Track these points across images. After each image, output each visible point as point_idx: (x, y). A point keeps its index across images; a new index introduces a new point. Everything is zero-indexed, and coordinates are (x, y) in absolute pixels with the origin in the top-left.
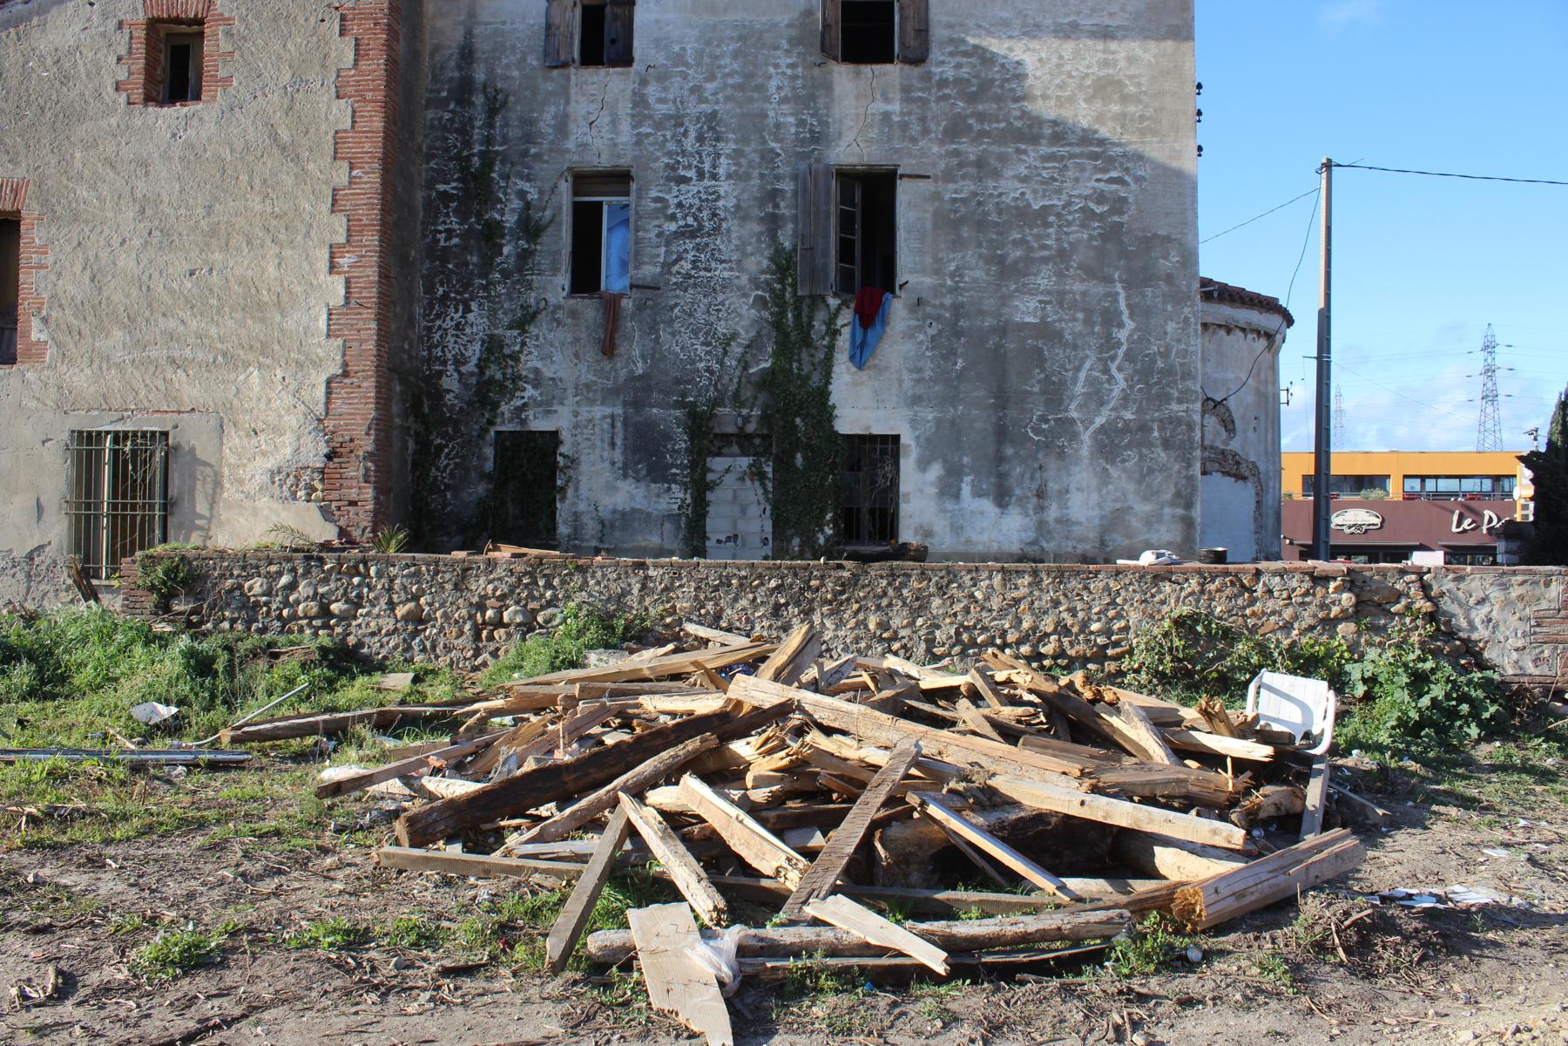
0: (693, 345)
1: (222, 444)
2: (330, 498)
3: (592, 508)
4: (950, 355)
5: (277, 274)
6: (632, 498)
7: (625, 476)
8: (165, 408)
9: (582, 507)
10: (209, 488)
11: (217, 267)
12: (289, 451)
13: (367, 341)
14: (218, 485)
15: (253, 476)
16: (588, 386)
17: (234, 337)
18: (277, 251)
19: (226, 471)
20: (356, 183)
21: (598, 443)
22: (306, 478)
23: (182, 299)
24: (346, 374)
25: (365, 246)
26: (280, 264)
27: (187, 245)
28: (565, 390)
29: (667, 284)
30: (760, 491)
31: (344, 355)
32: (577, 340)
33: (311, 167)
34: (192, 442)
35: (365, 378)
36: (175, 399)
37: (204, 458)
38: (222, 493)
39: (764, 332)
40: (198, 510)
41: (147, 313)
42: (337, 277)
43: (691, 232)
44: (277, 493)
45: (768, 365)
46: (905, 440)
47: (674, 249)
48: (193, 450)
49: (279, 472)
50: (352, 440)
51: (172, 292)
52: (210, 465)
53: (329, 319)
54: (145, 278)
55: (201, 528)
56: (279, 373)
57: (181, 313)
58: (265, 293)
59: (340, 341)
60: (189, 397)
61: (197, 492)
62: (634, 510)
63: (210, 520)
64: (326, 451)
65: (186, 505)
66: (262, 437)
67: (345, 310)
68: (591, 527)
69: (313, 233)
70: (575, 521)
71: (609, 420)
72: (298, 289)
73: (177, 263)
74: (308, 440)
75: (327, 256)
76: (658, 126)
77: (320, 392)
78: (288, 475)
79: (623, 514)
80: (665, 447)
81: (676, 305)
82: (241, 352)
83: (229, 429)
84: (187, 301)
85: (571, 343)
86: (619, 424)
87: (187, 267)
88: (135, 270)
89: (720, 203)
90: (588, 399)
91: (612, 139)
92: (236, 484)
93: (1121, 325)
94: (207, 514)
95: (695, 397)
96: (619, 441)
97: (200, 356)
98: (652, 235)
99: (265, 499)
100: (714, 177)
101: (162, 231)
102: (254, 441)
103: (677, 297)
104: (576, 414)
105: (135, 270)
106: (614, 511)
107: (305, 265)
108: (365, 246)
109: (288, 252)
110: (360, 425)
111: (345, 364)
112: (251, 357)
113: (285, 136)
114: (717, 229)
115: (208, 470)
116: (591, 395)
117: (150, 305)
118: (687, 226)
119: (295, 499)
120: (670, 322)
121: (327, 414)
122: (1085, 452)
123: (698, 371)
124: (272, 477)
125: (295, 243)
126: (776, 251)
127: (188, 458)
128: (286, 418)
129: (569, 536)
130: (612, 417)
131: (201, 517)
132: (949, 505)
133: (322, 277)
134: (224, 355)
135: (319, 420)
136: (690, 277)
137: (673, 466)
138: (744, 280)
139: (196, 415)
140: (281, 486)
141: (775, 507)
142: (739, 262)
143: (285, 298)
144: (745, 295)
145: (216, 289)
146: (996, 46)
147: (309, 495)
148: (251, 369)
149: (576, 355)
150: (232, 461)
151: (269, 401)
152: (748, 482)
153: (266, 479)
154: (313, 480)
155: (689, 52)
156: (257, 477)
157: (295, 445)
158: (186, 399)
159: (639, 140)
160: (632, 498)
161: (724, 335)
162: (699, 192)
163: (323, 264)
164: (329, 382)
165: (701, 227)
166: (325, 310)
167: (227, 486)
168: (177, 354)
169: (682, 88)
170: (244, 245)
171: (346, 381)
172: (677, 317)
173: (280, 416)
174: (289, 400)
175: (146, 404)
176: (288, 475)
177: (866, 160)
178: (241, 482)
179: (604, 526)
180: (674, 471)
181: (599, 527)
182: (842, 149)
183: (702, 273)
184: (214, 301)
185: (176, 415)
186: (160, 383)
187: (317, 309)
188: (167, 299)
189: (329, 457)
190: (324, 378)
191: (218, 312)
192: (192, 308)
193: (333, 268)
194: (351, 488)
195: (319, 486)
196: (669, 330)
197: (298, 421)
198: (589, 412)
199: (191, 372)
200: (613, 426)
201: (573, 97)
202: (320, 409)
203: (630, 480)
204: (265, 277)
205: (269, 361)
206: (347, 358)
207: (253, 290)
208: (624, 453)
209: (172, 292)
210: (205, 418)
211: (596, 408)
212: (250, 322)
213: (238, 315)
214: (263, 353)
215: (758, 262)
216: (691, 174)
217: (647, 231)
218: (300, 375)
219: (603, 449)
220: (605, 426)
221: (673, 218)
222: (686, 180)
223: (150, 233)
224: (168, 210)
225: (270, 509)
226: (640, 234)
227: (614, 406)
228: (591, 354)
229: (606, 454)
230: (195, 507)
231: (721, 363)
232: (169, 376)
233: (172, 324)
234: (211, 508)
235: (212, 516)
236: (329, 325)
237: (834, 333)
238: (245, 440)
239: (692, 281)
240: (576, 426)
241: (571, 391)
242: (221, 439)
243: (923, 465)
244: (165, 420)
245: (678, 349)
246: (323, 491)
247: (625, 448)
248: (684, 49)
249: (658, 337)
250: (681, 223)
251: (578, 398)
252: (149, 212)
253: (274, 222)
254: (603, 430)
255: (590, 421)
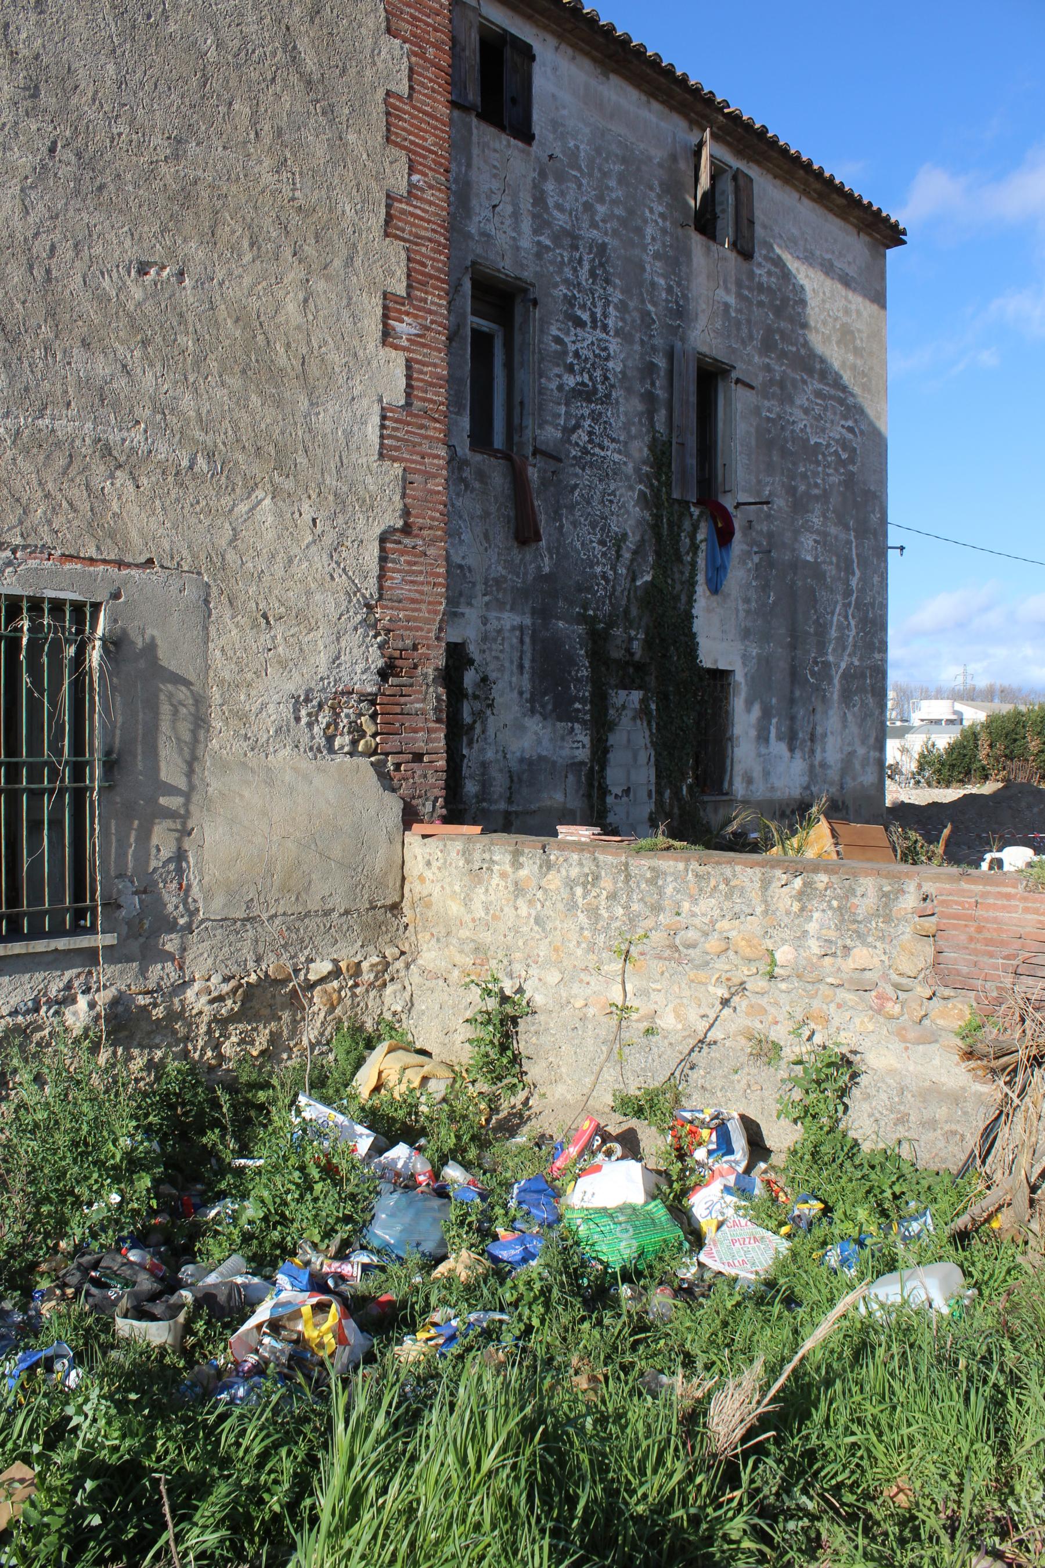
0: (592, 542)
1: (206, 640)
2: (387, 747)
3: (500, 756)
4: (765, 588)
5: (300, 320)
6: (539, 742)
7: (533, 711)
8: (92, 552)
9: (490, 755)
10: (184, 729)
11: (195, 270)
12: (322, 660)
13: (435, 476)
14: (200, 722)
15: (264, 706)
16: (498, 582)
17: (226, 424)
18: (302, 275)
19: (215, 694)
20: (417, 198)
21: (507, 664)
22: (347, 714)
23: (124, 321)
24: (407, 530)
25: (430, 312)
26: (306, 301)
27: (134, 205)
28: (474, 584)
29: (567, 456)
30: (647, 733)
31: (404, 496)
32: (486, 514)
33: (351, 137)
34: (149, 632)
35: (433, 541)
36: (112, 535)
37: (173, 666)
38: (208, 739)
39: (646, 537)
40: (163, 776)
41: (46, 332)
42: (394, 353)
43: (587, 392)
44: (305, 740)
45: (648, 578)
46: (739, 677)
47: (573, 411)
48: (151, 647)
49: (307, 700)
50: (415, 648)
51: (102, 299)
52: (187, 683)
53: (383, 427)
54: (40, 247)
55: (170, 814)
56: (308, 512)
57: (121, 349)
58: (281, 351)
59: (397, 469)
60: (140, 531)
61: (162, 740)
62: (541, 758)
63: (187, 796)
64: (380, 663)
65: (140, 766)
66: (279, 630)
67: (403, 416)
68: (499, 783)
69: (358, 262)
70: (483, 774)
71: (518, 633)
72: (336, 358)
73: (111, 236)
74: (352, 641)
75: (379, 311)
76: (556, 239)
77: (372, 552)
78: (320, 706)
79: (530, 763)
80: (569, 673)
81: (576, 486)
82: (241, 457)
83: (220, 609)
84: (134, 327)
85: (481, 517)
86: (527, 640)
87: (132, 252)
88: (17, 223)
89: (610, 364)
90: (497, 600)
91: (514, 239)
92: (234, 722)
93: (853, 574)
94: (181, 783)
95: (594, 610)
96: (527, 664)
97: (163, 451)
98: (553, 385)
99: (287, 752)
100: (605, 328)
101: (79, 155)
102: (265, 638)
103: (576, 475)
104: (485, 621)
105: (17, 223)
106: (522, 760)
107: (345, 314)
108: (430, 312)
109: (319, 285)
110: (428, 621)
111: (406, 513)
112: (256, 469)
113: (310, 63)
114: (608, 396)
115: (182, 693)
116: (500, 596)
117: (51, 314)
118: (583, 384)
119: (331, 750)
120: (571, 508)
121: (380, 598)
122: (836, 696)
123: (596, 577)
124: (296, 710)
125: (330, 270)
126: (654, 438)
127: (142, 664)
128: (318, 597)
129: (476, 796)
130: (521, 628)
131: (171, 790)
132: (763, 751)
133: (371, 346)
134: (210, 456)
135: (368, 606)
136: (587, 452)
137: (577, 699)
138: (629, 469)
139: (155, 575)
140: (310, 725)
141: (658, 755)
142: (626, 443)
143: (314, 369)
144: (631, 488)
145: (190, 317)
146: (793, 265)
147: (354, 743)
148: (259, 493)
149: (486, 536)
150: (227, 675)
151: (290, 561)
152: (638, 722)
153: (286, 711)
154: (360, 715)
155: (582, 154)
156: (271, 708)
157: (333, 649)
158: (134, 535)
159: (541, 251)
160: (539, 742)
161: (616, 534)
162: (593, 343)
163: (373, 326)
164: (383, 539)
165: (595, 391)
166: (376, 409)
167: (217, 724)
168: (114, 437)
169: (577, 200)
170: (246, 244)
171: (406, 541)
172: (578, 503)
173: (309, 593)
174: (321, 563)
175: (48, 539)
176: (320, 706)
177: (714, 353)
178: (243, 717)
179: (512, 781)
180: (577, 706)
181: (508, 780)
182: (698, 332)
183: (597, 450)
184: (187, 342)
185: (113, 571)
186: (78, 493)
187: (365, 402)
188: (89, 308)
189: (384, 674)
190: (378, 531)
191: (197, 364)
192: (145, 343)
193: (387, 335)
194: (415, 731)
195: (369, 728)
196: (571, 518)
197: (337, 605)
198: (499, 619)
199: (144, 481)
200: (522, 642)
201: (475, 161)
202: (370, 586)
203: (537, 717)
204: (281, 319)
205: (288, 485)
206: (408, 501)
207: (260, 338)
208: (532, 680)
209: (102, 299)
210: (175, 584)
211: (506, 615)
212: (255, 400)
213: (235, 382)
214: (279, 467)
215: (640, 449)
216: (585, 316)
217: (549, 379)
218: (340, 520)
219: (512, 674)
220: (515, 641)
221: (570, 369)
222: (579, 323)
223: (52, 150)
224: (91, 113)
225: (295, 769)
226: (543, 380)
227: (524, 613)
228: (501, 536)
229: (514, 679)
230: (156, 770)
231: (614, 568)
232: (96, 482)
233: (102, 368)
234: (190, 773)
235: (192, 787)
236: (382, 437)
237: (695, 548)
238: (250, 634)
239: (588, 457)
240: (485, 639)
241: (480, 588)
242: (206, 628)
243: (749, 704)
244: (94, 578)
245: (579, 546)
246: (374, 735)
247: (533, 674)
248: (577, 147)
249: (562, 526)
250: (579, 379)
251: (487, 598)
252: (48, 99)
253: (295, 219)
254: (512, 646)
255: (499, 631)
